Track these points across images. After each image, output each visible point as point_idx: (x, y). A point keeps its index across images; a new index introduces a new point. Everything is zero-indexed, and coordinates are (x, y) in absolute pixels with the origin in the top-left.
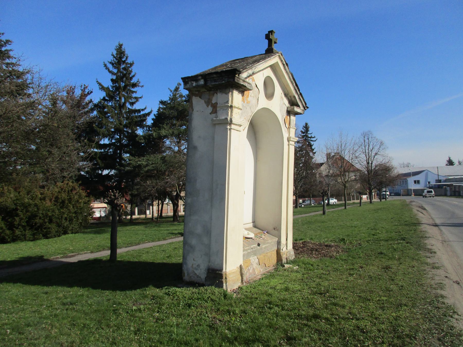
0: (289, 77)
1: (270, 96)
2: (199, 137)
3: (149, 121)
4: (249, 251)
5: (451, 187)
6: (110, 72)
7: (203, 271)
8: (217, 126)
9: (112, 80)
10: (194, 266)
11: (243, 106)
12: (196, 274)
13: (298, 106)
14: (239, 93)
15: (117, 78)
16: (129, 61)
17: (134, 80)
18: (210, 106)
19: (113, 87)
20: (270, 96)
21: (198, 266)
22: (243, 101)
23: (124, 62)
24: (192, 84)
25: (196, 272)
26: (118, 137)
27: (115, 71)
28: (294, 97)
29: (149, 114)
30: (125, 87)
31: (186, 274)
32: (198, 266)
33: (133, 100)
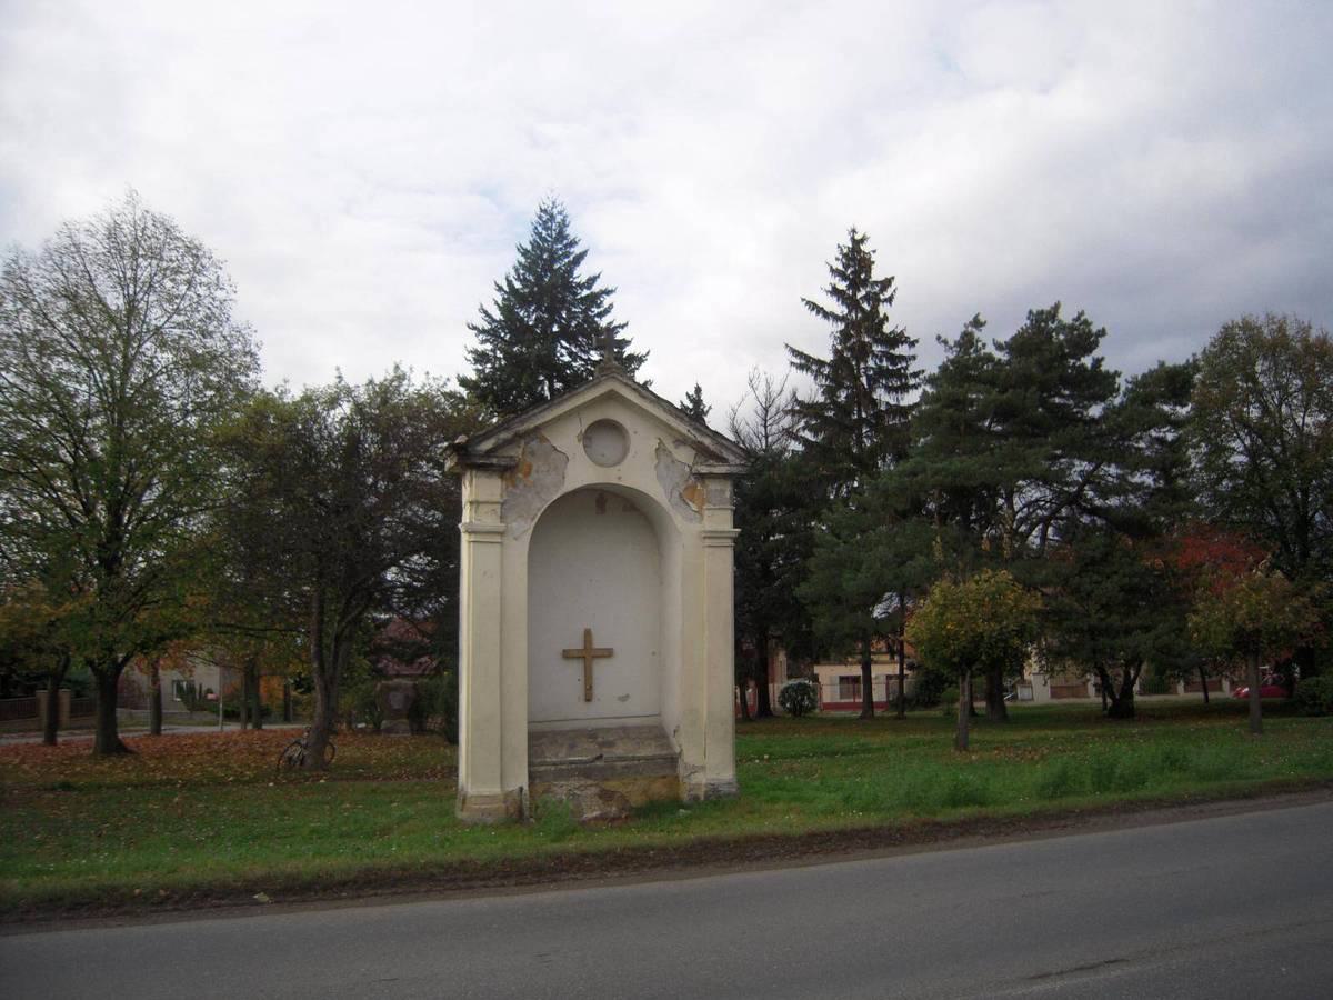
6: (827, 315)
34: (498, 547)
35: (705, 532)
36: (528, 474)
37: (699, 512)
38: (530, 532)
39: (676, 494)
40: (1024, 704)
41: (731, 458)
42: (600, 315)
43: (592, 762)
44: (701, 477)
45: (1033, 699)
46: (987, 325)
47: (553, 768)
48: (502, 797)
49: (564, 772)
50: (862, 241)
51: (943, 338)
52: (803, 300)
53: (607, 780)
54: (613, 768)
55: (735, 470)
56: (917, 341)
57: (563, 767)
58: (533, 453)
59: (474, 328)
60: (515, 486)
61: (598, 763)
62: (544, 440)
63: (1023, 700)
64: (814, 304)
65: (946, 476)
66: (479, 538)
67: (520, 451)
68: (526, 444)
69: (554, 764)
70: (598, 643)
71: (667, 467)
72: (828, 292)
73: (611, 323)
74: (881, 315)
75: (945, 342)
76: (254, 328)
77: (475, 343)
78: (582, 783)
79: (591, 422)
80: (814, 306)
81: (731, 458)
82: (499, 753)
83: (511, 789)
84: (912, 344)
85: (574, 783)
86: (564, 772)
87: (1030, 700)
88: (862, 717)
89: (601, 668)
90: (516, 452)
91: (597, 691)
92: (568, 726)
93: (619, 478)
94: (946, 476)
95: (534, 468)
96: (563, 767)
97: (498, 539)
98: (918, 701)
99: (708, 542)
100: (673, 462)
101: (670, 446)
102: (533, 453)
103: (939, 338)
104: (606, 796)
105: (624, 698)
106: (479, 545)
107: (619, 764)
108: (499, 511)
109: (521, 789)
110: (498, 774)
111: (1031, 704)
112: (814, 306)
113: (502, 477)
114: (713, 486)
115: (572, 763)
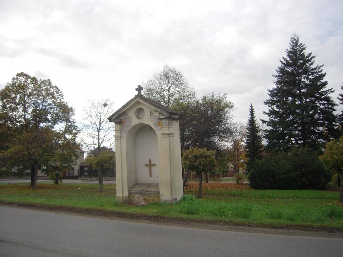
34: (119, 140)
35: (162, 133)
36: (125, 123)
37: (161, 128)
38: (126, 136)
39: (155, 124)
41: (165, 113)
42: (310, 65)
43: (142, 191)
44: (161, 119)
47: (134, 192)
48: (122, 197)
49: (136, 193)
53: (145, 196)
54: (146, 193)
55: (165, 117)
57: (136, 192)
58: (125, 118)
59: (274, 76)
60: (123, 126)
61: (143, 192)
62: (127, 115)
66: (165, 136)
67: (123, 118)
68: (124, 116)
69: (134, 191)
70: (148, 163)
71: (153, 118)
76: (194, 89)
77: (276, 79)
78: (140, 196)
79: (137, 108)
81: (165, 113)
82: (121, 187)
83: (125, 195)
85: (138, 196)
86: (136, 193)
89: (153, 168)
90: (122, 118)
91: (153, 175)
92: (147, 182)
93: (143, 122)
95: (126, 121)
96: (136, 192)
97: (119, 138)
99: (163, 136)
100: (154, 116)
101: (153, 112)
102: (125, 118)
104: (145, 200)
105: (158, 176)
107: (147, 192)
108: (120, 132)
109: (127, 196)
110: (122, 192)
113: (120, 125)
114: (164, 121)
115: (137, 191)
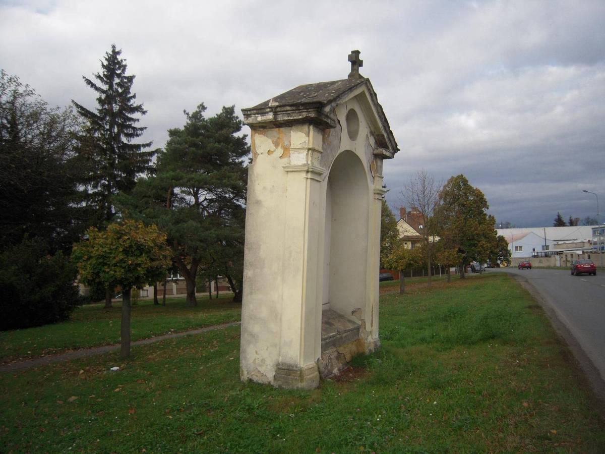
0: (378, 110)
1: (353, 135)
2: (264, 188)
3: (153, 161)
4: (327, 341)
5: (561, 256)
6: (97, 89)
7: (269, 367)
8: (289, 174)
9: (100, 100)
10: (257, 361)
11: (323, 148)
12: (259, 371)
13: (388, 148)
14: (194, 113)
15: (107, 97)
16: (127, 74)
17: (134, 103)
18: (280, 147)
19: (100, 111)
20: (353, 135)
21: (263, 360)
22: (324, 142)
23: (119, 76)
24: (257, 117)
25: (259, 369)
26: (107, 183)
27: (105, 87)
28: (383, 136)
29: (151, 154)
30: (120, 111)
31: (245, 373)
32: (262, 361)
33: (130, 131)
40: (144, 299)
45: (148, 296)
46: (236, 106)
50: (119, 53)
51: (187, 112)
52: (84, 77)
56: (146, 112)
63: (144, 297)
64: (90, 81)
65: (195, 182)
72: (96, 76)
73: (106, 59)
74: (132, 95)
75: (188, 114)
80: (89, 82)
84: (144, 113)
87: (146, 297)
88: (105, 308)
94: (195, 182)
98: (92, 299)
103: (185, 111)
106: (315, 182)
111: (147, 298)
112: (89, 82)
